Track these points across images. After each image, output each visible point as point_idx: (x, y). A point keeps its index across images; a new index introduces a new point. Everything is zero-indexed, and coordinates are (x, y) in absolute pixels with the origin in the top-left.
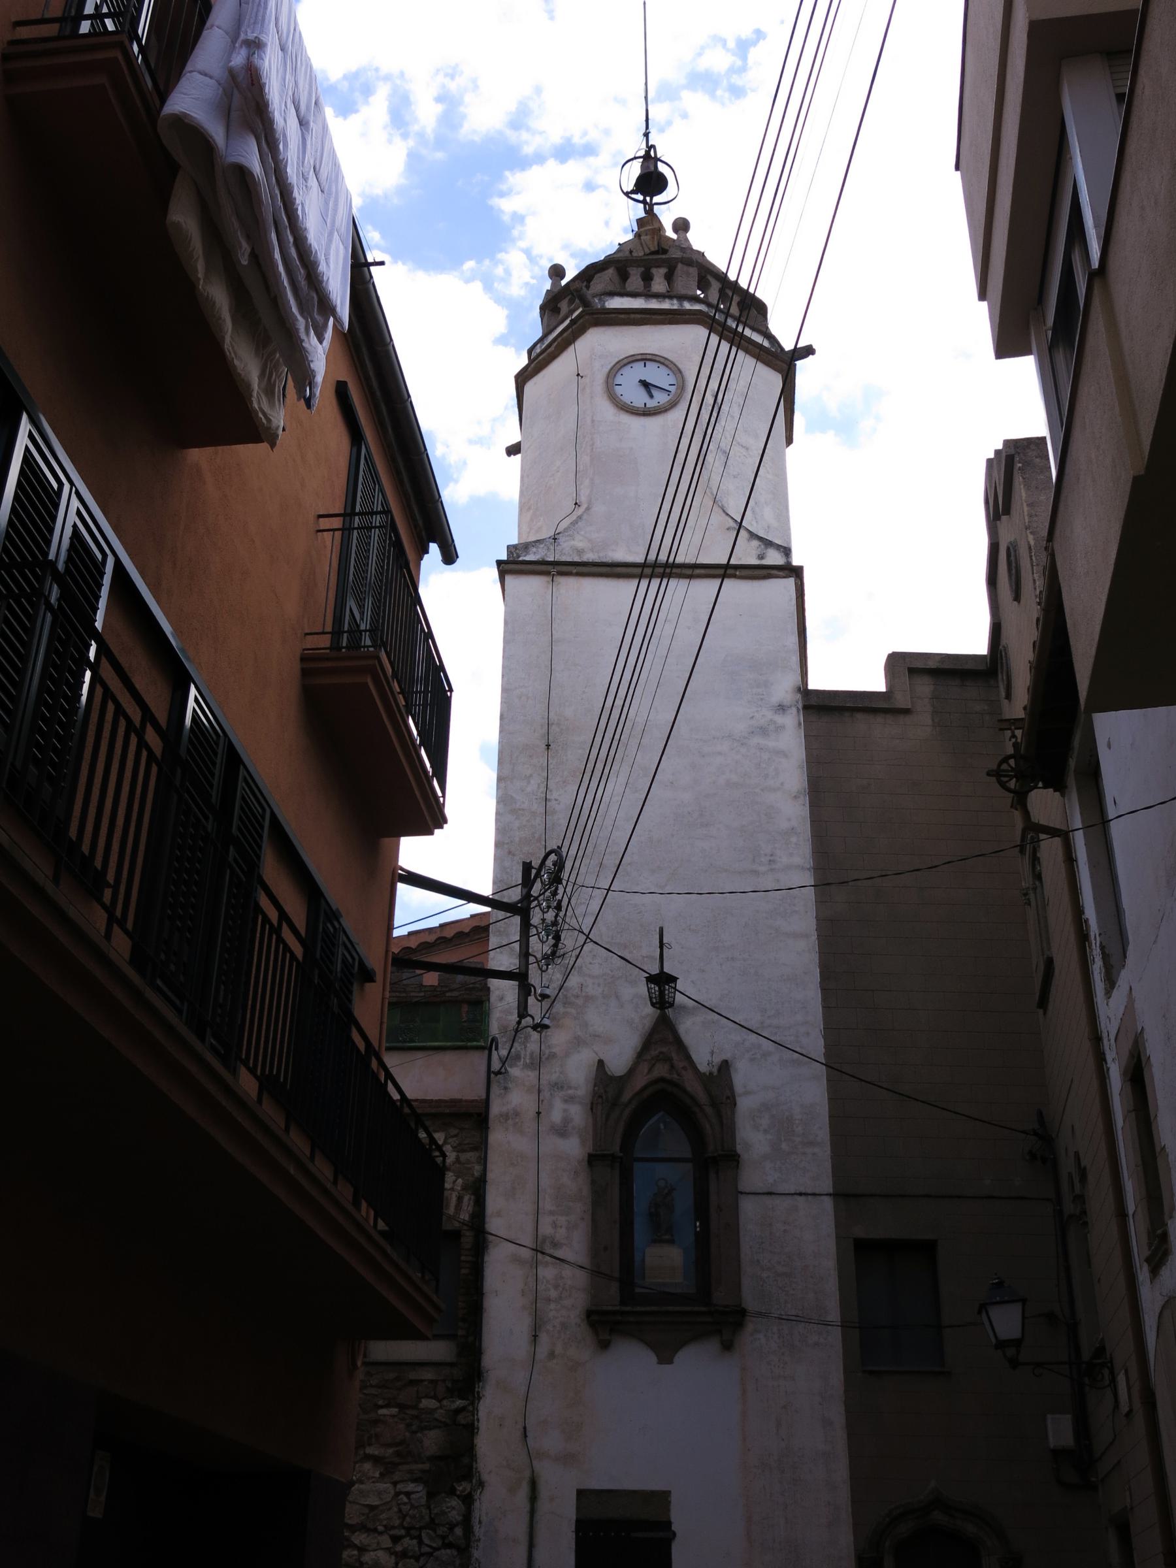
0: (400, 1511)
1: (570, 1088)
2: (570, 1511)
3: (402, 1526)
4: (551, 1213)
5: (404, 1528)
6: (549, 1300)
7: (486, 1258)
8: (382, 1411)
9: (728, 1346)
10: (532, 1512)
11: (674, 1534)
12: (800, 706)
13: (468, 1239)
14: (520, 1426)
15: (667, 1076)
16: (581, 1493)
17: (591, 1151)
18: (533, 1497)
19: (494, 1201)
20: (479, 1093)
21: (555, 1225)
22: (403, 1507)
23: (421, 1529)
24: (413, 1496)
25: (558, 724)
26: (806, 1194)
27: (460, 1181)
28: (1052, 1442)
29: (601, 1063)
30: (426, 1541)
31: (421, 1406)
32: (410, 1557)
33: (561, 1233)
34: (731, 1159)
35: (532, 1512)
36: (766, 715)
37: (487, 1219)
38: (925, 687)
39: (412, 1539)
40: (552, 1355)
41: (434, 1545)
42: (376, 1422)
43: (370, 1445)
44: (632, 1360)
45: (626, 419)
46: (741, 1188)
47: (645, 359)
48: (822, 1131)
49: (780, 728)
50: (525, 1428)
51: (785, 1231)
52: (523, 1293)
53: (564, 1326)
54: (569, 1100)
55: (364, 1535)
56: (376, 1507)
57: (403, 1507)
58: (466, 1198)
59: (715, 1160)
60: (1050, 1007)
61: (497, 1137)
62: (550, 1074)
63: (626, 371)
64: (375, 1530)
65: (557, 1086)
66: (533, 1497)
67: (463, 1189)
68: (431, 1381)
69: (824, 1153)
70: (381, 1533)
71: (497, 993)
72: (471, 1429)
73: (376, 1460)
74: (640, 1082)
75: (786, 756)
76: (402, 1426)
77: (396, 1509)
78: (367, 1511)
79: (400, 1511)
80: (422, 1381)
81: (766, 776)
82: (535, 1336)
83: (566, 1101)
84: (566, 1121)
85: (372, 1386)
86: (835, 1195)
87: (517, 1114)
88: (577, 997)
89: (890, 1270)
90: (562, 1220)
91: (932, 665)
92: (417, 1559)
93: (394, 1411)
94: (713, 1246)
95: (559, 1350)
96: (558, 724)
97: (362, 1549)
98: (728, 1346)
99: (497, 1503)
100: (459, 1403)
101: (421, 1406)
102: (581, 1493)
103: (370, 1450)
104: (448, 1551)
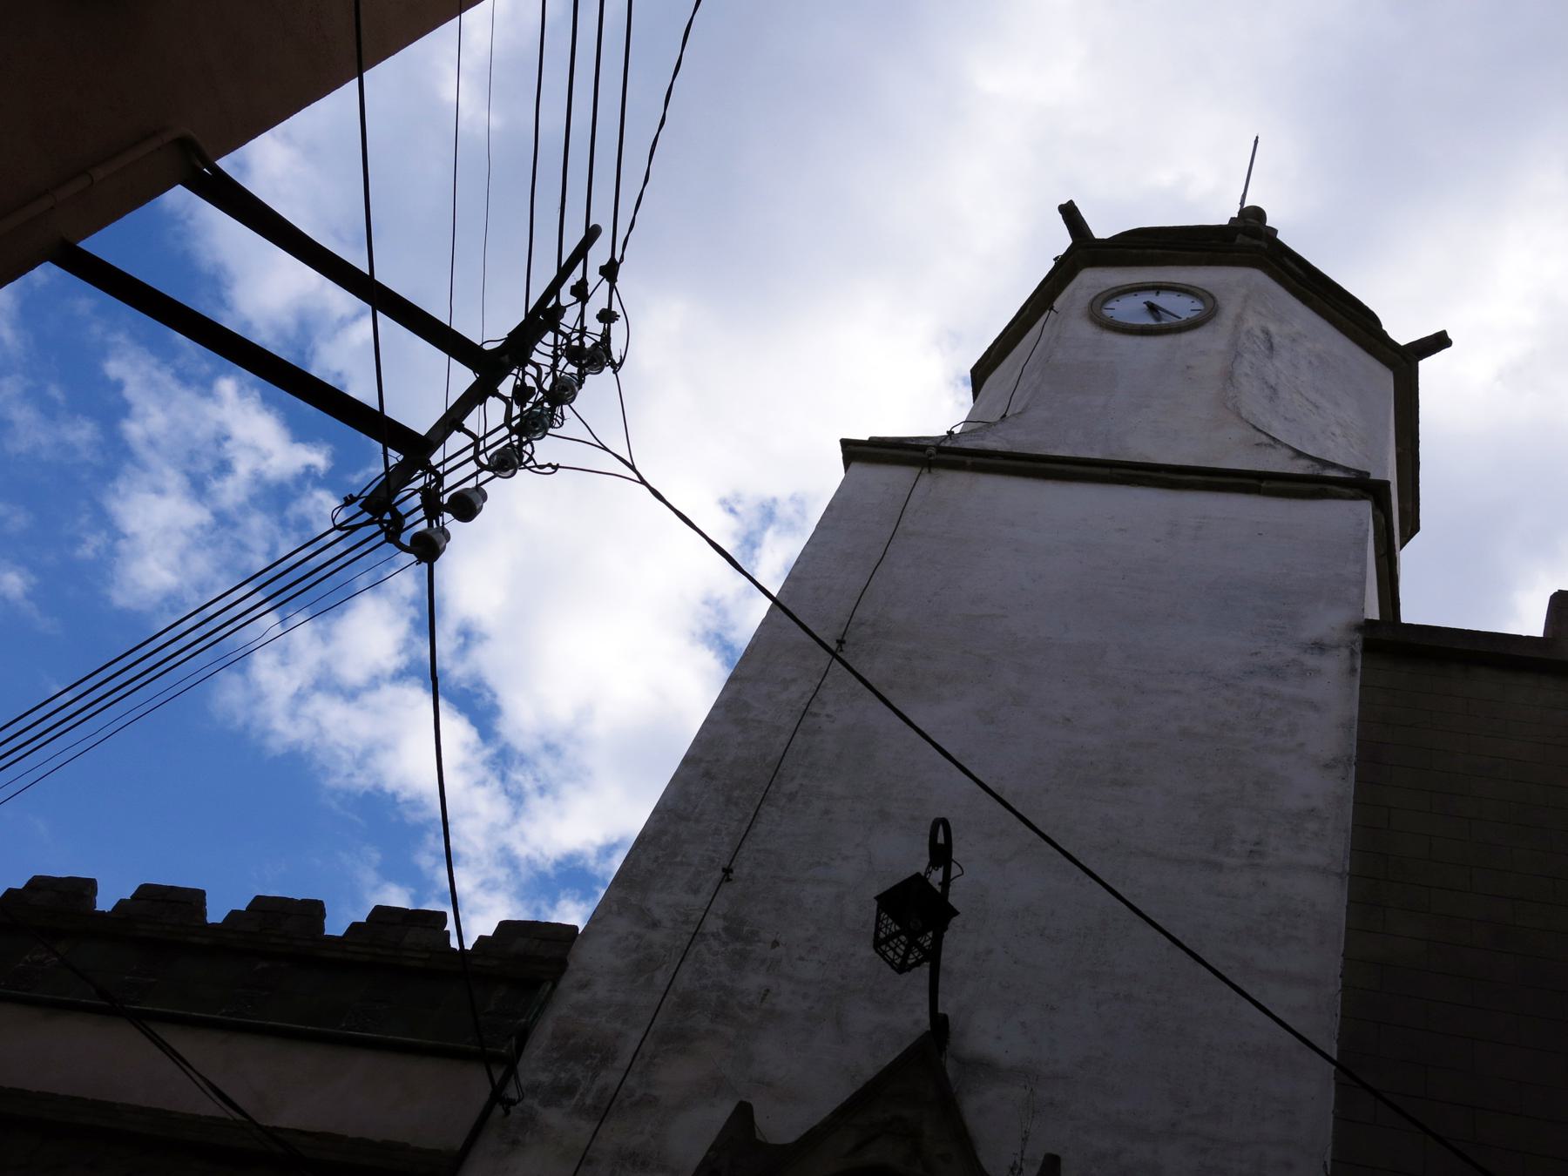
12: (1358, 648)
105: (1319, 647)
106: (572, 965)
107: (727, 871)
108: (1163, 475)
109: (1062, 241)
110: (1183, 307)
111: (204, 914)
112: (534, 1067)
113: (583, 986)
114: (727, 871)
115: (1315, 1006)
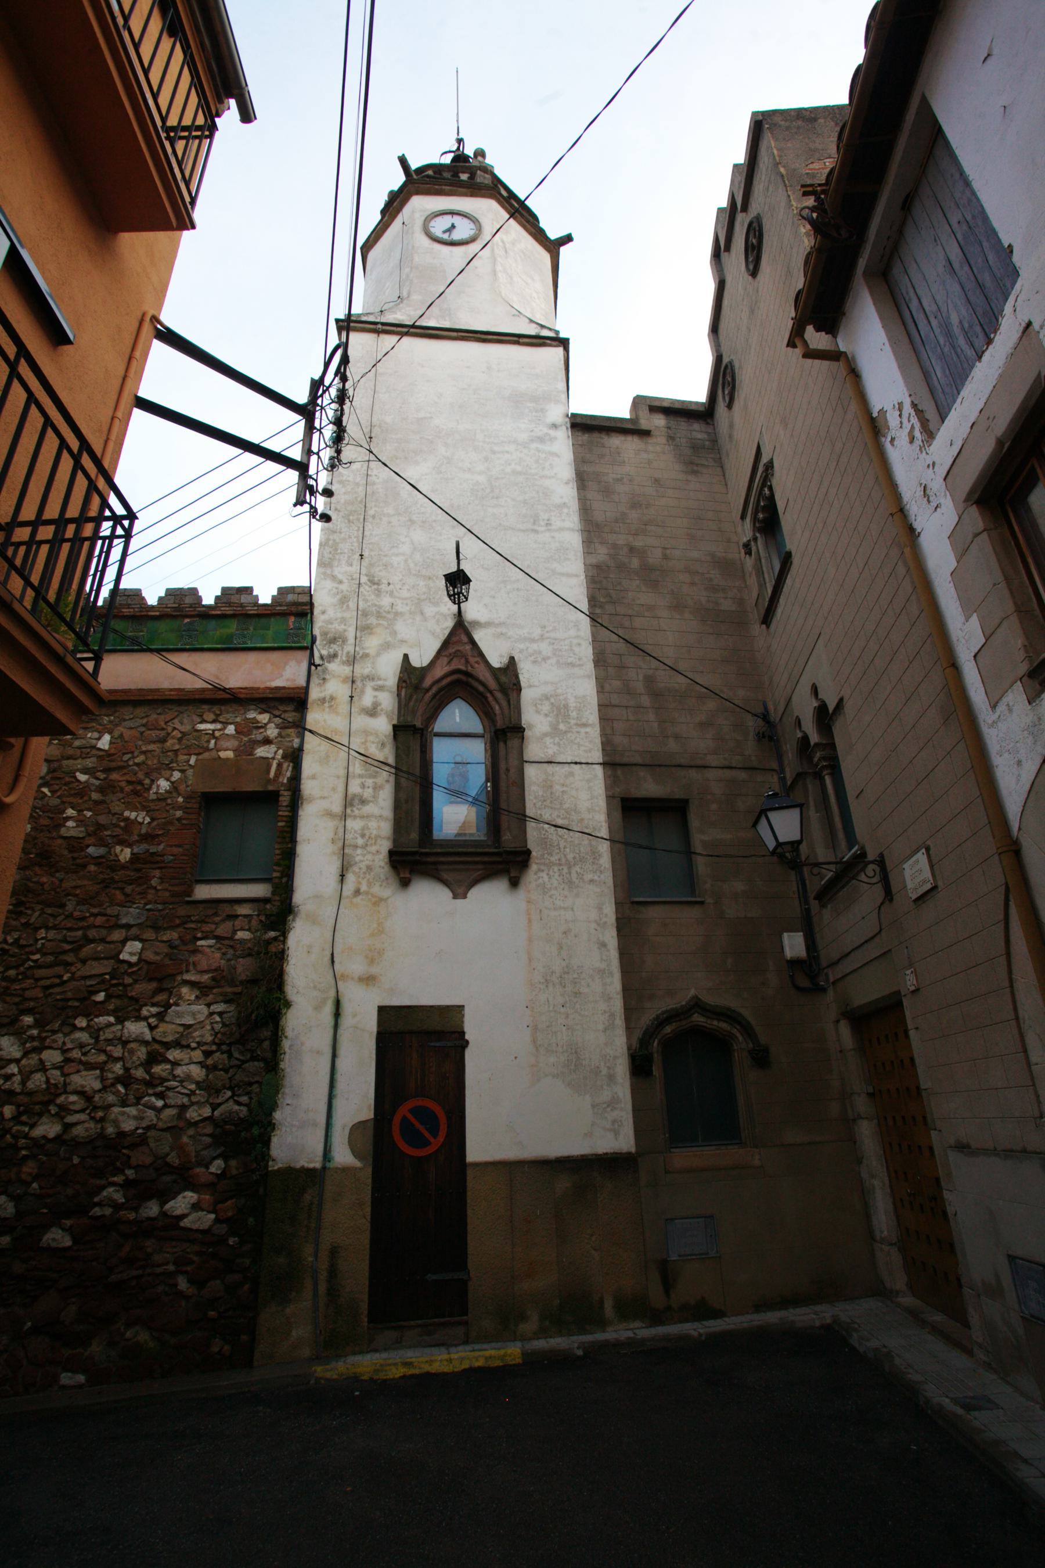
0: (213, 1029)
1: (380, 679)
2: (371, 1024)
3: (214, 1043)
4: (360, 776)
5: (215, 1044)
6: (356, 847)
7: (300, 813)
8: (199, 943)
9: (514, 883)
10: (336, 1026)
11: (467, 1042)
12: (569, 425)
13: (285, 798)
14: (328, 953)
15: (463, 668)
16: (382, 1010)
17: (395, 722)
18: (337, 1014)
19: (309, 766)
20: (302, 682)
21: (363, 786)
22: (215, 1025)
23: (230, 1045)
24: (225, 1015)
25: (380, 426)
26: (581, 763)
27: (281, 752)
28: (789, 953)
29: (406, 657)
30: (236, 1055)
31: (237, 937)
32: (221, 1070)
33: (368, 793)
34: (518, 730)
35: (336, 1026)
36: (542, 430)
37: (303, 781)
38: (659, 421)
39: (222, 1053)
40: (357, 892)
41: (242, 1058)
42: (196, 951)
43: (187, 971)
44: (428, 897)
45: (437, 247)
46: (525, 759)
47: (452, 213)
48: (592, 715)
49: (552, 439)
50: (332, 955)
51: (563, 792)
52: (333, 841)
53: (369, 868)
54: (379, 689)
55: (178, 1051)
56: (190, 1026)
57: (215, 1025)
58: (285, 765)
59: (505, 734)
60: (773, 626)
61: (314, 717)
62: (363, 669)
63: (439, 219)
64: (188, 1046)
65: (370, 678)
66: (337, 1014)
67: (283, 758)
68: (245, 916)
69: (594, 733)
70: (194, 1049)
71: (320, 608)
72: (281, 956)
73: (193, 984)
74: (439, 672)
75: (557, 456)
76: (218, 955)
77: (209, 1027)
78: (181, 1029)
79: (213, 1029)
80: (237, 916)
81: (543, 468)
82: (342, 876)
83: (376, 690)
84: (376, 705)
85: (192, 921)
86: (604, 764)
87: (332, 698)
88: (389, 612)
89: (647, 817)
90: (370, 782)
91: (665, 404)
92: (226, 1071)
93: (212, 942)
94: (503, 797)
95: (364, 888)
96: (380, 426)
97: (176, 1064)
98: (514, 883)
99: (304, 1022)
100: (272, 934)
101: (237, 937)
102: (382, 1010)
103: (187, 977)
104: (256, 1063)
105: (555, 426)
106: (316, 604)
107: (361, 555)
108: (479, 336)
109: (400, 178)
110: (463, 230)
111: (840, 108)
112: (321, 649)
113: (323, 612)
114: (361, 555)
115: (576, 589)
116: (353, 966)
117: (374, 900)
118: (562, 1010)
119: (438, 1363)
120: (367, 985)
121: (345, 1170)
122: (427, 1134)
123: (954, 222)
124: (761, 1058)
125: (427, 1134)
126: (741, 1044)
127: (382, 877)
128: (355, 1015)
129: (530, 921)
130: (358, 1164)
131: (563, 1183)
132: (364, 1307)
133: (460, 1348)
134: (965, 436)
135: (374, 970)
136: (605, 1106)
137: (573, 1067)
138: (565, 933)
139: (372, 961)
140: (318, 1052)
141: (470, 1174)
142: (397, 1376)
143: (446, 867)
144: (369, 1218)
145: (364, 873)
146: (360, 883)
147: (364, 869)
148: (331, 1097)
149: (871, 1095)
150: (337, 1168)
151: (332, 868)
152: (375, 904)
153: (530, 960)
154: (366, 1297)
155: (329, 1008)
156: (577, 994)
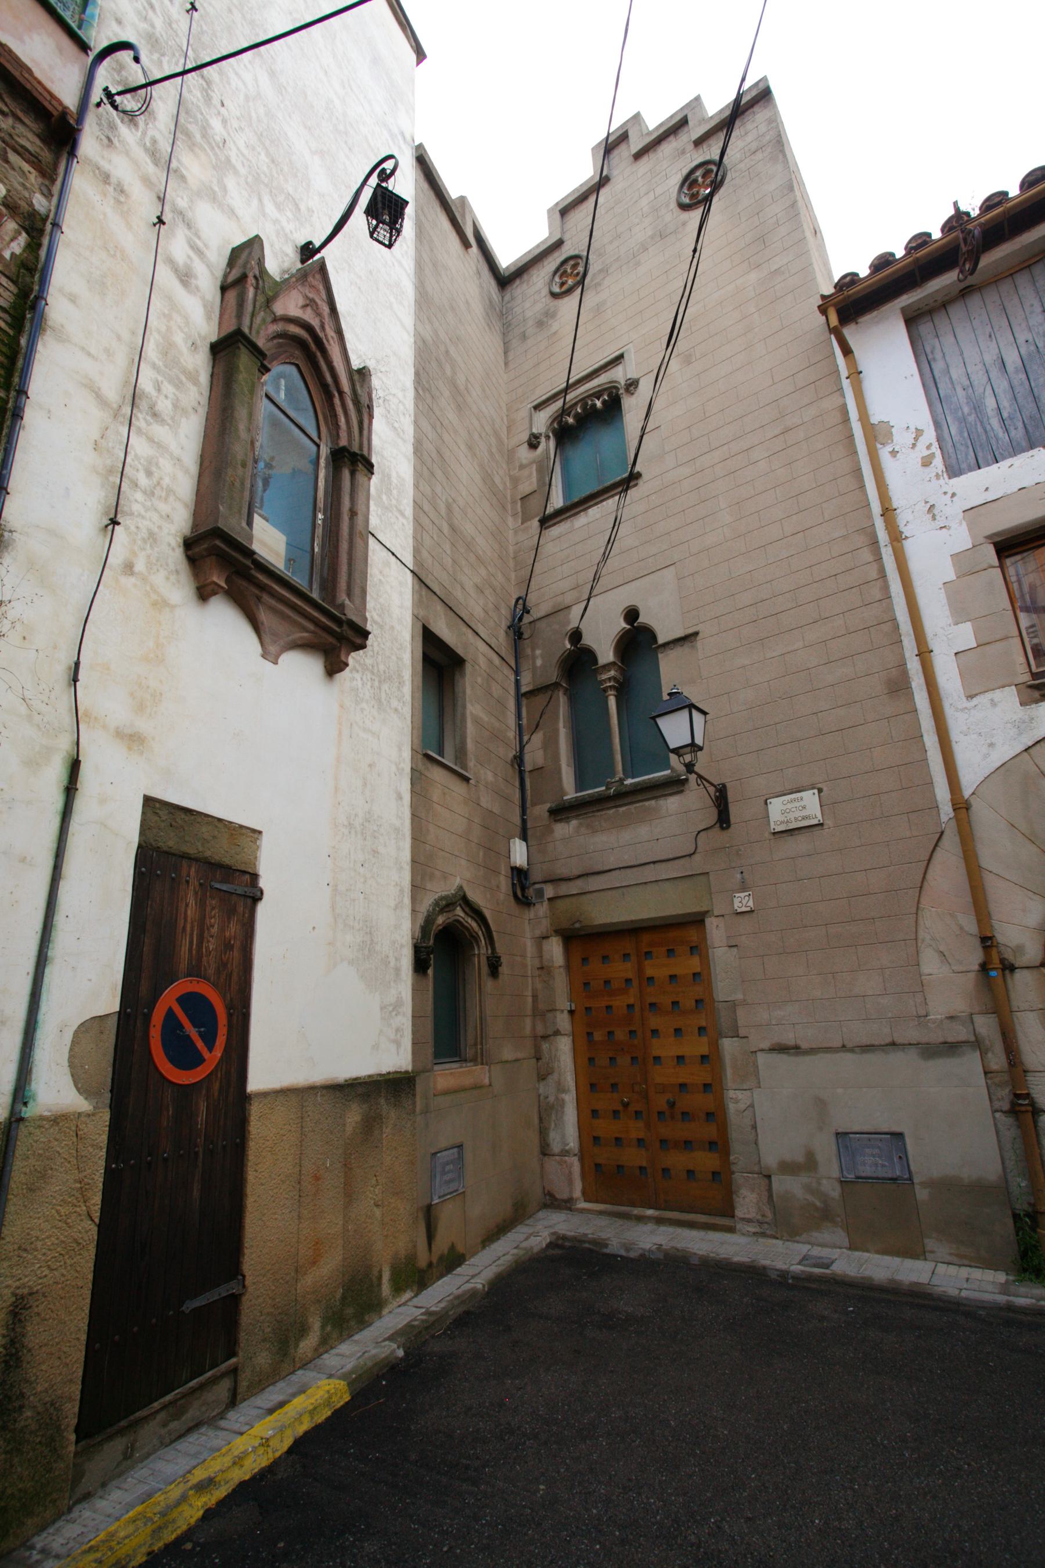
18: (71, 789)
33: (164, 406)
40: (128, 568)
50: (77, 664)
66: (71, 789)
95: (140, 566)
116: (105, 699)
117: (154, 597)
118: (362, 870)
119: (252, 1457)
120: (130, 749)
121: (58, 1120)
122: (200, 1044)
123: (1021, 339)
124: (494, 966)
125: (200, 1044)
126: (482, 950)
127: (172, 567)
128: (103, 801)
129: (340, 733)
130: (80, 1104)
131: (354, 1116)
132: (71, 1410)
133: (235, 1418)
134: (1009, 492)
135: (143, 725)
136: (391, 1008)
137: (366, 952)
138: (370, 766)
139: (140, 708)
140: (23, 860)
141: (255, 1110)
142: (193, 1521)
143: (273, 602)
144: (96, 1216)
145: (144, 541)
146: (135, 554)
147: (144, 534)
148: (42, 961)
149: (571, 1012)
150: (42, 1118)
151: (89, 502)
152: (155, 604)
153: (336, 789)
154: (76, 1390)
155: (55, 773)
156: (375, 852)
